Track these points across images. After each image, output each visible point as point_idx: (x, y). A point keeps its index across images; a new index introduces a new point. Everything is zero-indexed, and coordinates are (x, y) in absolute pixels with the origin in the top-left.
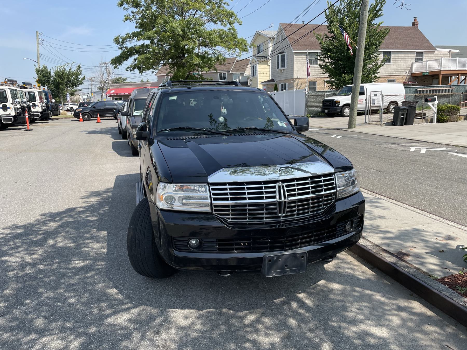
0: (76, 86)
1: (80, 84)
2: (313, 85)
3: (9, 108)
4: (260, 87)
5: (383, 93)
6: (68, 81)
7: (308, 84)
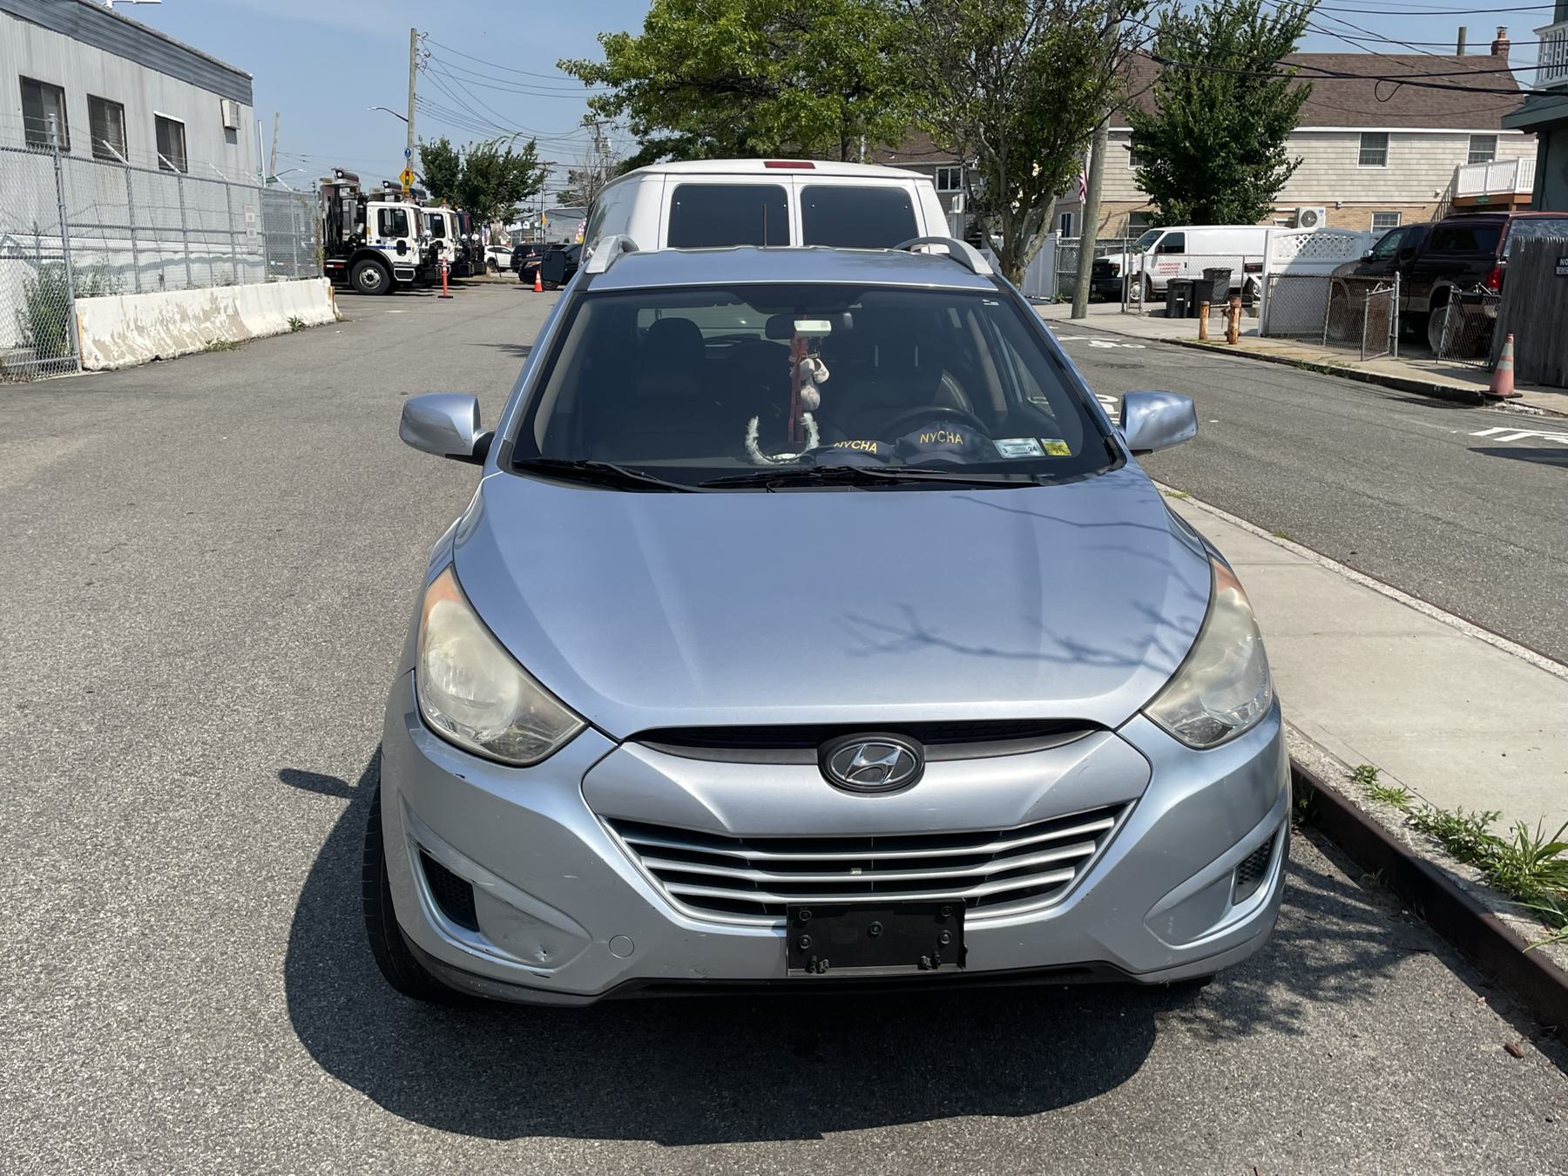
0: (519, 199)
1: (529, 194)
3: (409, 249)
6: (500, 185)
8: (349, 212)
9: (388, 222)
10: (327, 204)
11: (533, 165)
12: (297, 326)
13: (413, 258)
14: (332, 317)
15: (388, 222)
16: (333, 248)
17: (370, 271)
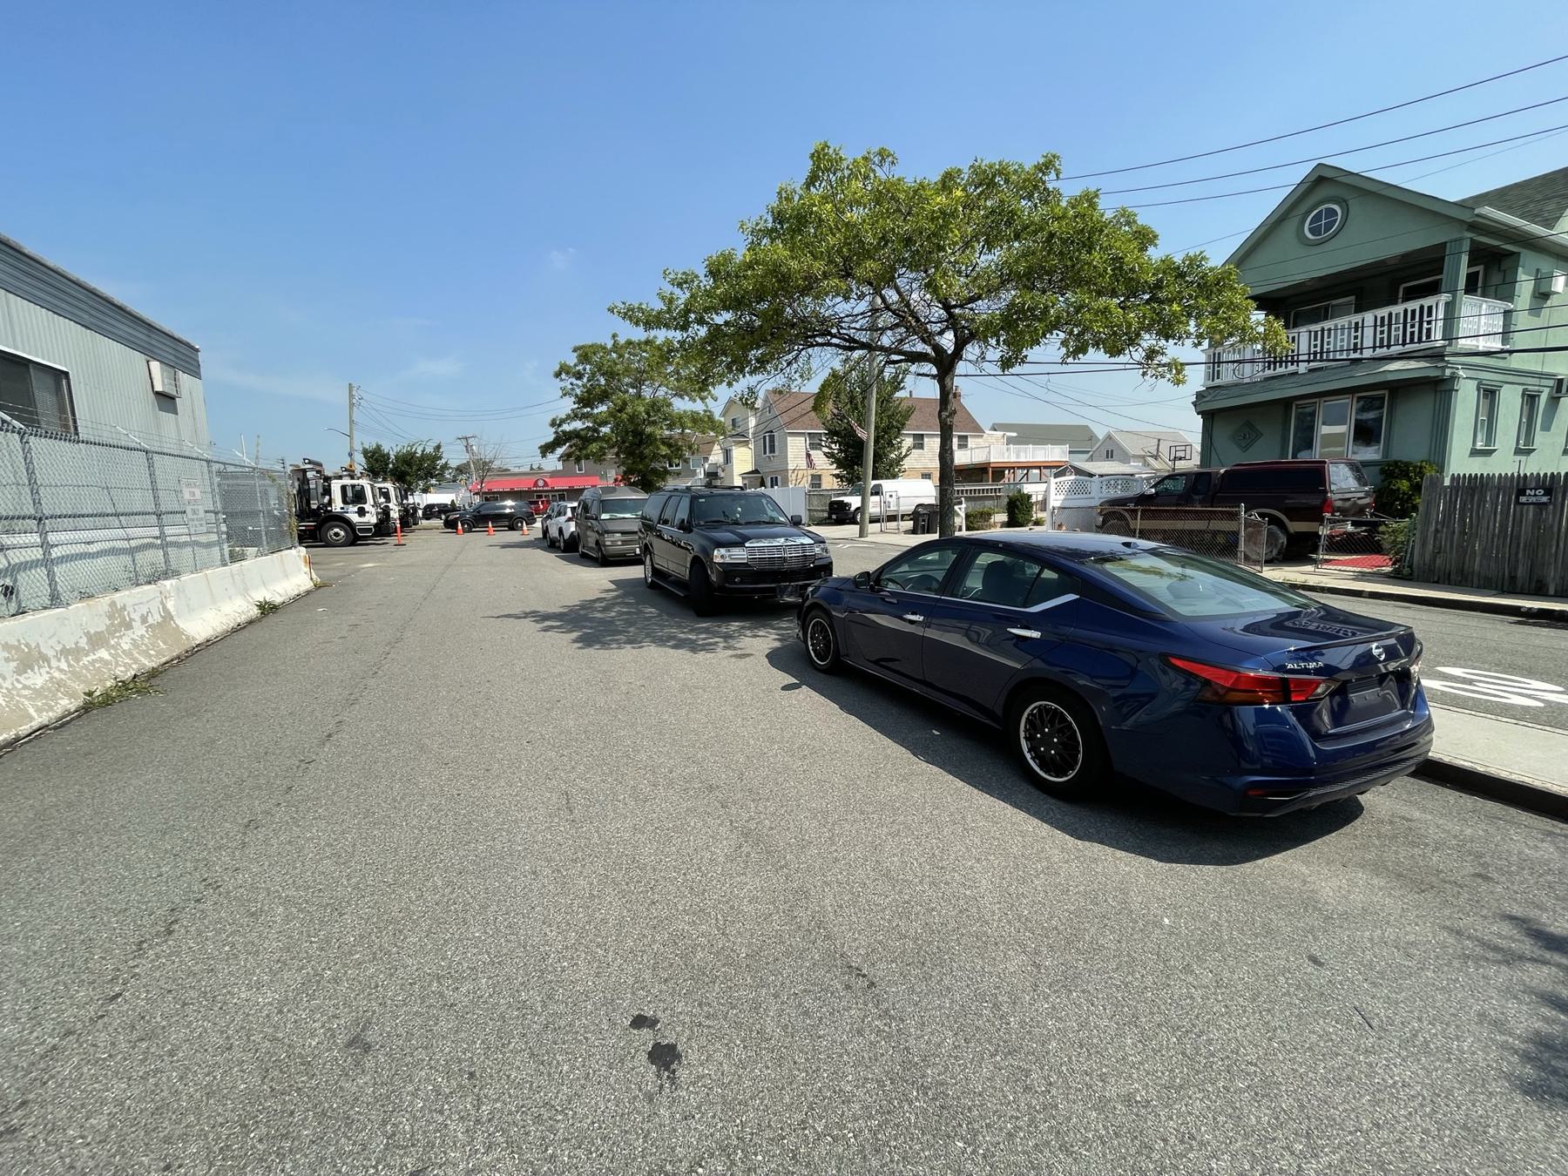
2: (816, 480)
4: (738, 482)
5: (900, 495)
7: (810, 478)
8: (316, 489)
9: (350, 494)
10: (297, 484)
11: (440, 458)
12: (267, 609)
13: (371, 519)
14: (309, 585)
15: (350, 494)
16: (304, 514)
17: (336, 530)
